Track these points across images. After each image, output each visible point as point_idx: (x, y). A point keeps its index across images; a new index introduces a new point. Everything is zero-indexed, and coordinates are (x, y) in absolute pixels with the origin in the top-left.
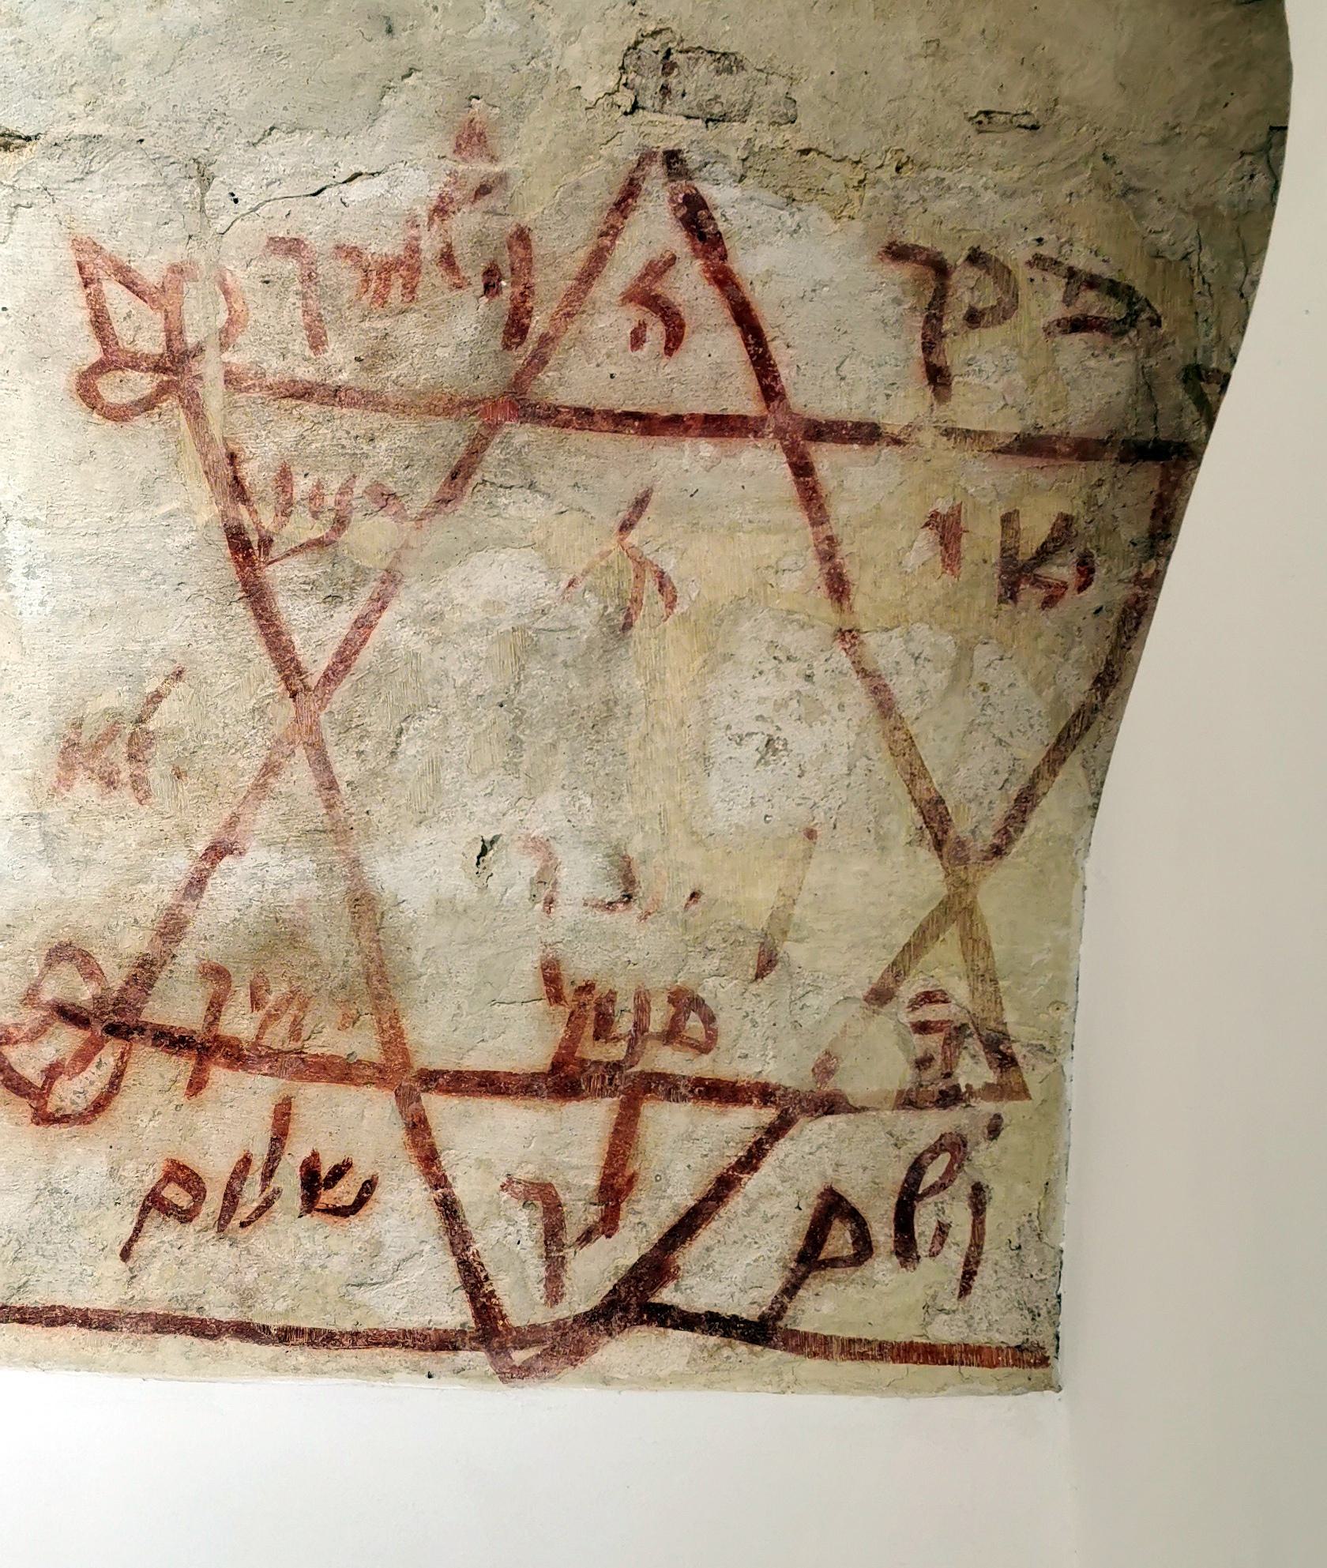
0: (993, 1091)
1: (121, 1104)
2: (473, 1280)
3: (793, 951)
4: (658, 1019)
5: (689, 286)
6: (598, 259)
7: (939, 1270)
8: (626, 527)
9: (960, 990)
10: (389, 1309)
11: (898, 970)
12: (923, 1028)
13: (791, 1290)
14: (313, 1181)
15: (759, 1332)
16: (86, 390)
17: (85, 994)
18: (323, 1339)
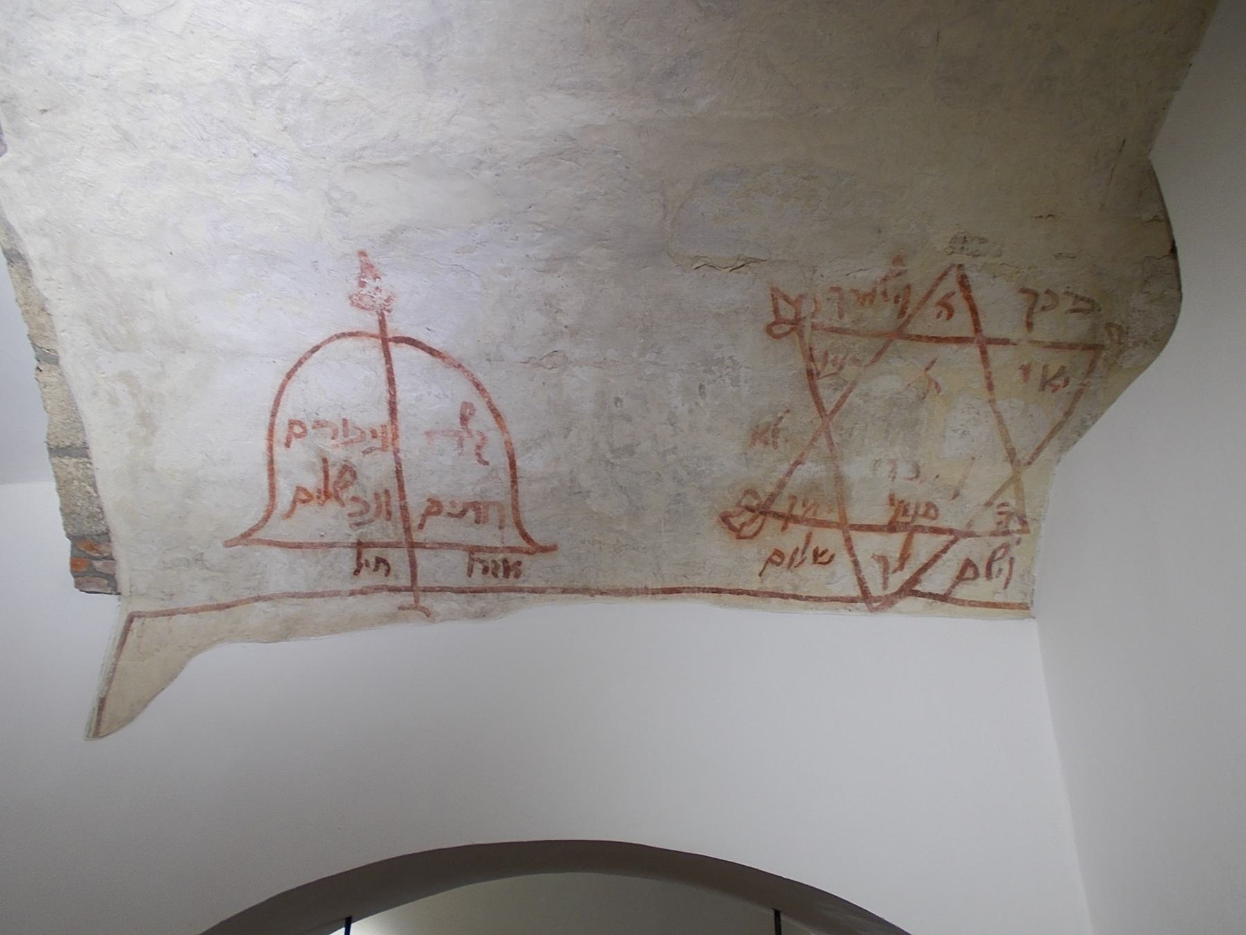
0: (1019, 531)
1: (762, 533)
2: (861, 582)
3: (963, 492)
4: (922, 510)
5: (958, 301)
6: (931, 292)
7: (998, 582)
8: (927, 369)
9: (1013, 503)
10: (836, 590)
11: (995, 496)
12: (1000, 513)
13: (953, 587)
14: (816, 555)
15: (944, 598)
16: (769, 329)
17: (755, 503)
18: (819, 599)
